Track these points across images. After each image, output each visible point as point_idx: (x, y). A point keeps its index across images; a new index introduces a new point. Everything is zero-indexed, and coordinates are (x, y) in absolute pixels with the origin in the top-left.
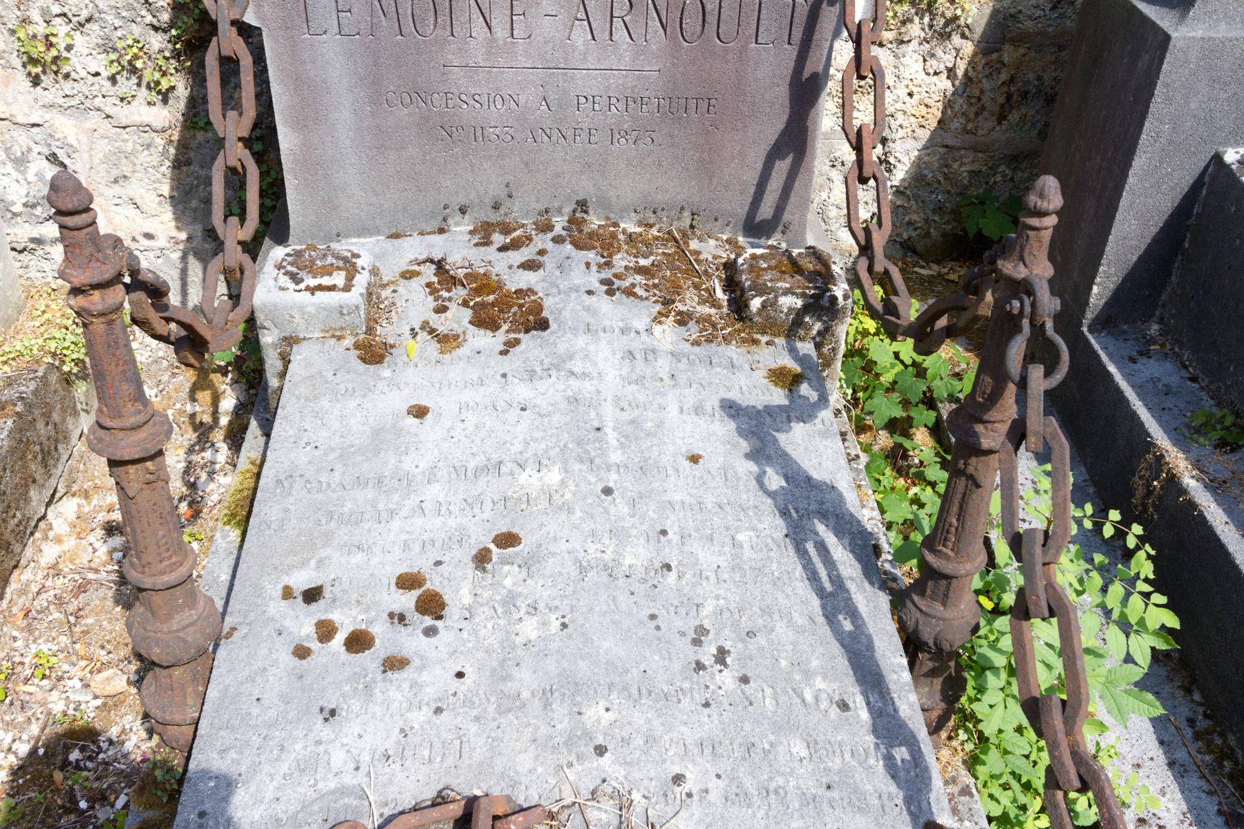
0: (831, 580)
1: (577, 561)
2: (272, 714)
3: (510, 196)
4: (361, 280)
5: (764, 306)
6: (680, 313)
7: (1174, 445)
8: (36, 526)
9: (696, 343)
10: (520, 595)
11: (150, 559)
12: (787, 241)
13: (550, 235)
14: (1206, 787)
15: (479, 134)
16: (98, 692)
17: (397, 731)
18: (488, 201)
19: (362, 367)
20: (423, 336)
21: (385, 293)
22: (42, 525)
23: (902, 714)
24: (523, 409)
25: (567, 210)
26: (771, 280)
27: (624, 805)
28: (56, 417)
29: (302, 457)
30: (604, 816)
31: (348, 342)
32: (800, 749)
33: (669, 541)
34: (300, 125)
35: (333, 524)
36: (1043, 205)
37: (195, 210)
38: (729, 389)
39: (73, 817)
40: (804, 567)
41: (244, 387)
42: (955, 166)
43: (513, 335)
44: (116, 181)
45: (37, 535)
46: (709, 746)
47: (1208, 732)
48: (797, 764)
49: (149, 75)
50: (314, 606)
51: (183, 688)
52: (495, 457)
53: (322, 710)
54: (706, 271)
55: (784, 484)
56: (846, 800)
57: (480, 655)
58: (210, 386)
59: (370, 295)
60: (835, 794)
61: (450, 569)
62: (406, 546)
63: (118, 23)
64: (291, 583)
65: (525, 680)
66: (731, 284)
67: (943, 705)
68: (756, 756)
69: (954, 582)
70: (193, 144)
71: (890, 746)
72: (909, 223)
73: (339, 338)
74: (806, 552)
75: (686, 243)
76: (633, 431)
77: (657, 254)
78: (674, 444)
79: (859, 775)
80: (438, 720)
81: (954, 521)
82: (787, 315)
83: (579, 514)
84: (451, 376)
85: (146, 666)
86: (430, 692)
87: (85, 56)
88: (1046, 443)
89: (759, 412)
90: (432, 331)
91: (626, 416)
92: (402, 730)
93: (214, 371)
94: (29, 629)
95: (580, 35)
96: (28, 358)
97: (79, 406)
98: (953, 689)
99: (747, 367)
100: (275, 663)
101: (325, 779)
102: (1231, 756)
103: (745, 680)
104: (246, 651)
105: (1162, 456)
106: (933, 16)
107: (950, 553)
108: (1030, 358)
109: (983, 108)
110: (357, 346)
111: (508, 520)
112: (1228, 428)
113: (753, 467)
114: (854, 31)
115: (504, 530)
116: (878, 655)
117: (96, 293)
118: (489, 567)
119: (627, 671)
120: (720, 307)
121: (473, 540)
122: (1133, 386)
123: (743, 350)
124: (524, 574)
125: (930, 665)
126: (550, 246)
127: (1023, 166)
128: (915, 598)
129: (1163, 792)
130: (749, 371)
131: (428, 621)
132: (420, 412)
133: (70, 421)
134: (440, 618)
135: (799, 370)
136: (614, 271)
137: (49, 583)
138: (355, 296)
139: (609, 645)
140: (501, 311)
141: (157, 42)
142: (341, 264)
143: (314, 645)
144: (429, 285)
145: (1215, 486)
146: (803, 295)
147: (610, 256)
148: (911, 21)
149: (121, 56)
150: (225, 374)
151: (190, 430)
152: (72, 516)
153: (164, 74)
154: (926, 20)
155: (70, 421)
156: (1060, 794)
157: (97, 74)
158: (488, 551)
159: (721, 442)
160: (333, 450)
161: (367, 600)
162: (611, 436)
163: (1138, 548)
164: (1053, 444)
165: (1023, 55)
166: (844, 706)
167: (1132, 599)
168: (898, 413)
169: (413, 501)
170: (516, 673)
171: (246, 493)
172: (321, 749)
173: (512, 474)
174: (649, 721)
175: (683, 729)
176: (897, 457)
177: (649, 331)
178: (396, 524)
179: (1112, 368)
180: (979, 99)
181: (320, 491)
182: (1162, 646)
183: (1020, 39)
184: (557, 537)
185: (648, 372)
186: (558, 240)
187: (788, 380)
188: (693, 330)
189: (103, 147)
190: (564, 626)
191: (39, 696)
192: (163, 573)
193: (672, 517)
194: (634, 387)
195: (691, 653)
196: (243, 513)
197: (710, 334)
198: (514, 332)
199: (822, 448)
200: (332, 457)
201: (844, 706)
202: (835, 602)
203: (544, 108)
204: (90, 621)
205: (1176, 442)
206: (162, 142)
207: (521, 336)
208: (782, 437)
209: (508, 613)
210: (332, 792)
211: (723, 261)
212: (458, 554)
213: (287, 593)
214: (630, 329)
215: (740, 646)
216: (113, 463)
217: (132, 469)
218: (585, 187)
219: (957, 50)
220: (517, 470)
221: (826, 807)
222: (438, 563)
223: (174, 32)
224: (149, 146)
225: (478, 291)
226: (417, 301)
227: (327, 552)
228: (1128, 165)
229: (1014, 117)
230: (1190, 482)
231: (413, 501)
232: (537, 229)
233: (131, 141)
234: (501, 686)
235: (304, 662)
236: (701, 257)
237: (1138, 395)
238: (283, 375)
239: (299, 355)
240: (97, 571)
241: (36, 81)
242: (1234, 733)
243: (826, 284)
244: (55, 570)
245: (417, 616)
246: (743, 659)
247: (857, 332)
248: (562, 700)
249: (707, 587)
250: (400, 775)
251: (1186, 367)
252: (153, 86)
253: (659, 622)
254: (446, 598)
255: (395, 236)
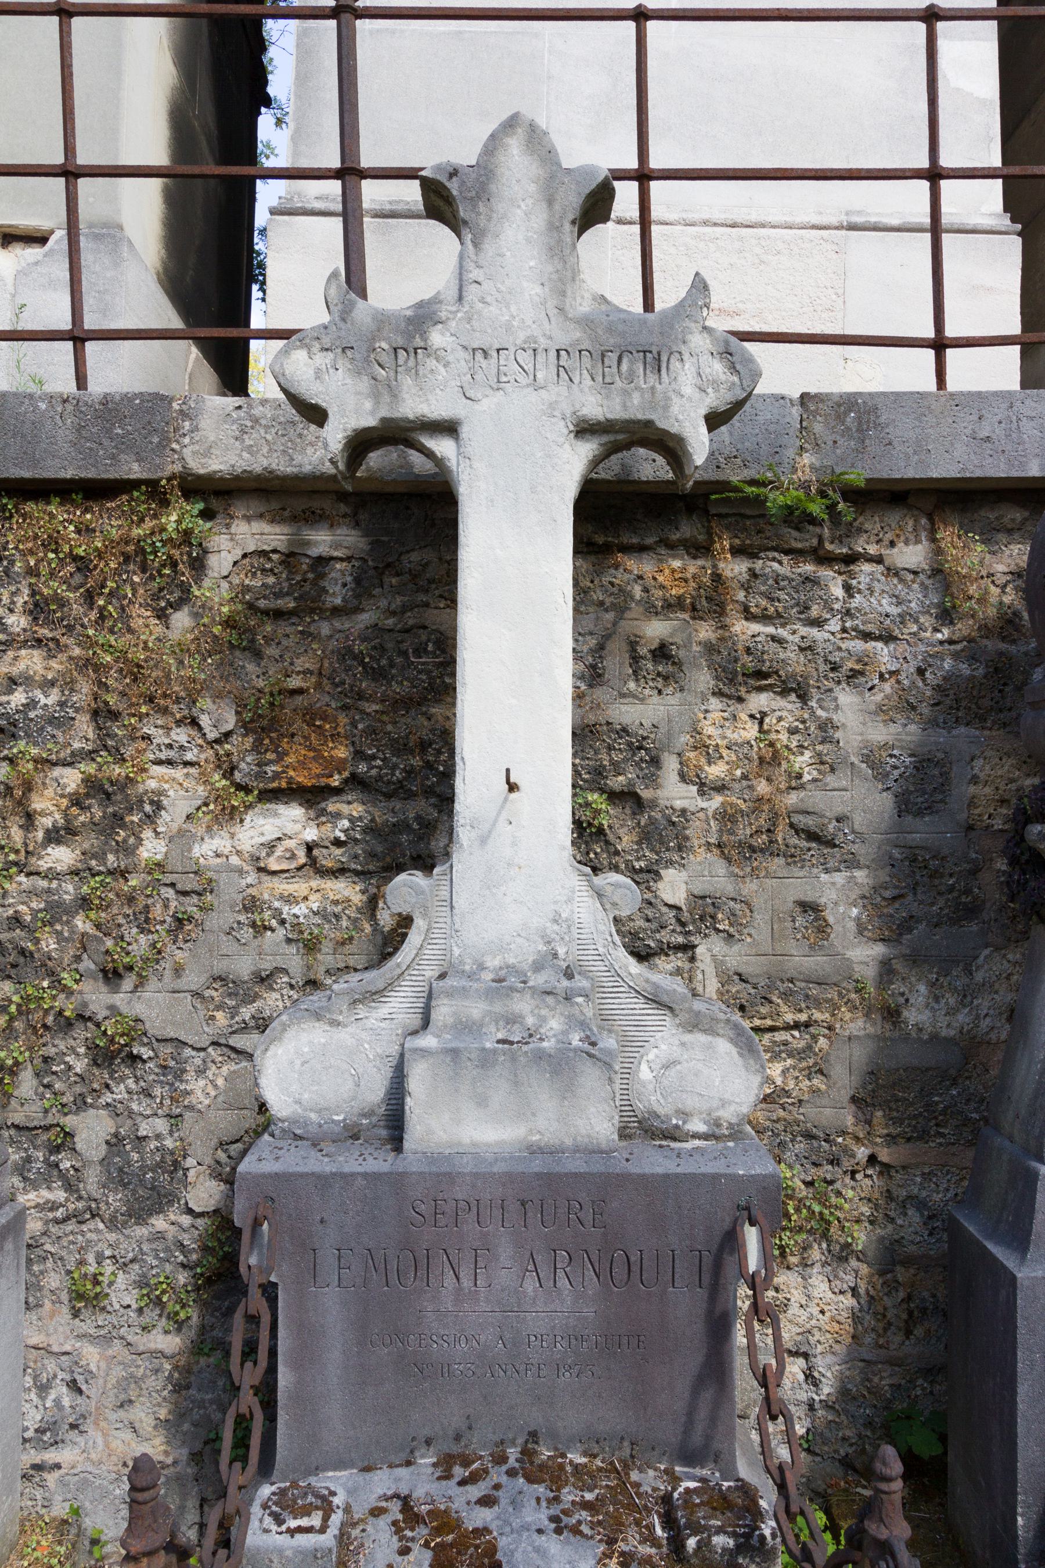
3: (470, 1428)
4: (336, 1519)
6: (623, 1554)
12: (720, 1471)
13: (504, 1468)
15: (445, 1370)
18: (451, 1433)
21: (355, 1532)
25: (520, 1441)
26: (704, 1518)
34: (298, 1365)
36: (887, 1472)
37: (185, 1434)
42: (876, 1379)
44: (122, 1406)
49: (172, 1307)
54: (646, 1506)
59: (343, 1538)
63: (155, 1263)
66: (669, 1521)
70: (195, 1369)
72: (844, 1439)
75: (627, 1474)
77: (601, 1487)
82: (722, 1555)
87: (122, 1292)
95: (530, 1285)
106: (829, 1242)
109: (890, 1324)
114: (750, 1281)
117: (145, 1560)
126: (504, 1479)
127: (940, 1378)
136: (561, 1506)
138: (327, 1539)
140: (459, 1553)
141: (182, 1278)
142: (319, 1503)
144: (395, 1523)
146: (734, 1535)
147: (559, 1490)
148: (810, 1247)
149: (152, 1291)
153: (183, 1307)
154: (824, 1245)
157: (129, 1306)
165: (915, 1275)
180: (884, 1316)
183: (907, 1262)
186: (511, 1473)
189: (118, 1372)
203: (501, 1346)
206: (169, 1367)
211: (662, 1493)
218: (535, 1418)
219: (856, 1272)
223: (199, 1270)
224: (157, 1371)
225: (438, 1531)
226: (383, 1541)
228: (1014, 1393)
229: (919, 1331)
232: (493, 1461)
233: (142, 1368)
236: (642, 1490)
241: (76, 1314)
243: (754, 1521)
252: (172, 1317)
255: (367, 1469)
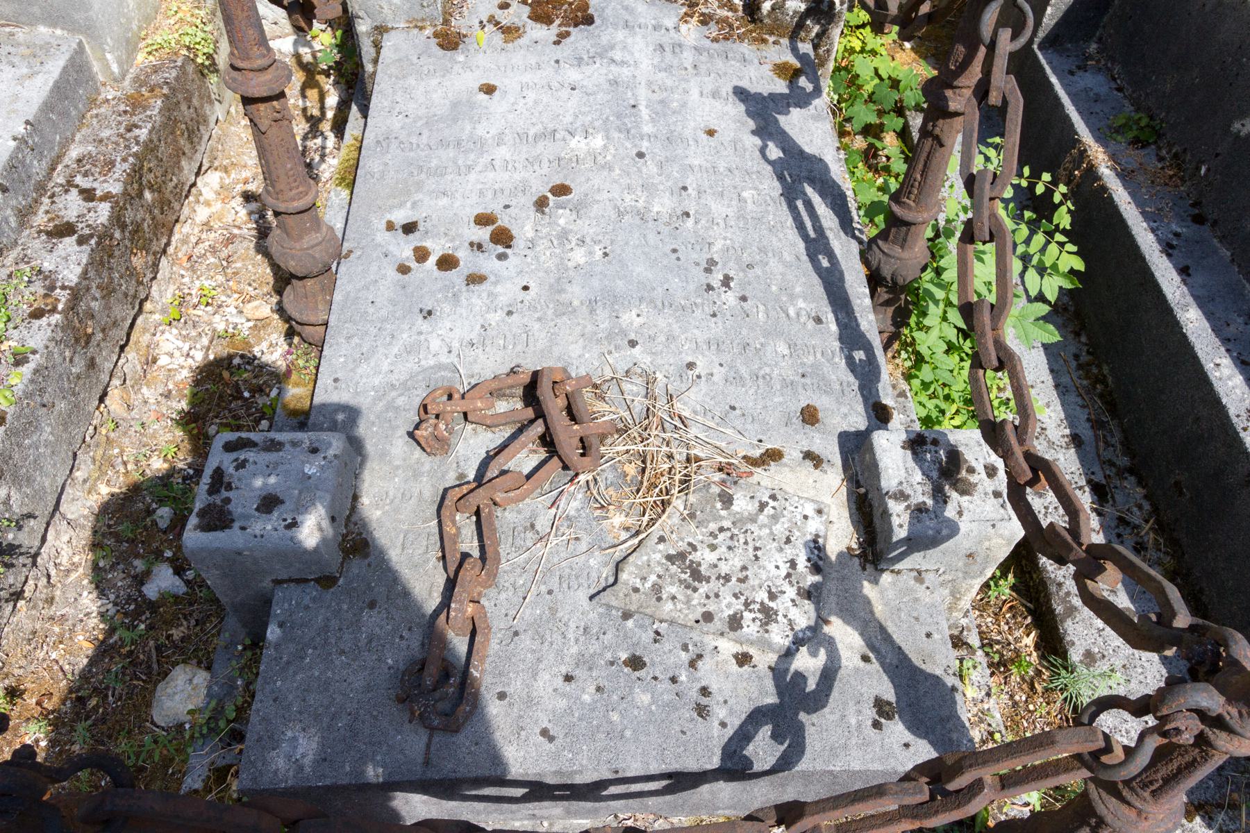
0: (815, 230)
1: (616, 207)
2: (384, 313)
5: (773, 8)
6: (703, 14)
7: (1097, 141)
8: (189, 191)
9: (715, 40)
10: (571, 231)
11: (282, 187)
14: (1080, 402)
16: (250, 316)
17: (479, 326)
19: (441, 52)
20: (490, 28)
22: (193, 190)
23: (862, 328)
24: (573, 89)
27: (650, 381)
28: (195, 102)
29: (396, 123)
30: (635, 388)
31: (429, 31)
32: (783, 349)
33: (689, 195)
35: (423, 176)
38: (740, 78)
39: (240, 403)
40: (794, 219)
41: (344, 87)
43: (564, 29)
45: (191, 198)
46: (716, 345)
47: (1088, 364)
48: (780, 359)
50: (411, 236)
51: (314, 296)
52: (551, 126)
53: (421, 311)
55: (782, 155)
56: (816, 386)
57: (541, 274)
58: (317, 85)
60: (808, 381)
61: (516, 211)
62: (481, 193)
64: (393, 219)
65: (576, 293)
67: (892, 329)
68: (750, 352)
69: (913, 228)
71: (851, 349)
73: (421, 28)
74: (796, 207)
76: (661, 109)
78: (695, 120)
79: (827, 369)
80: (510, 320)
81: (919, 177)
82: (792, 18)
83: (617, 172)
84: (514, 61)
85: (283, 280)
86: (503, 300)
88: (1004, 97)
89: (764, 98)
90: (497, 23)
91: (656, 97)
92: (483, 326)
93: (319, 73)
94: (193, 269)
96: (167, 50)
97: (213, 97)
98: (901, 319)
99: (756, 61)
100: (384, 277)
101: (426, 359)
102: (1103, 381)
103: (744, 299)
104: (361, 268)
105: (1085, 150)
107: (912, 203)
108: (1000, 24)
110: (436, 35)
111: (561, 175)
112: (1142, 128)
113: (758, 142)
115: (558, 182)
116: (847, 285)
118: (547, 210)
119: (654, 289)
120: (736, 11)
121: (534, 190)
122: (1069, 94)
123: (754, 47)
124: (574, 216)
125: (886, 296)
128: (880, 242)
129: (1048, 405)
130: (760, 67)
131: (500, 249)
132: (489, 90)
133: (207, 107)
134: (509, 247)
135: (799, 65)
137: (204, 236)
139: (640, 270)
140: (554, 8)
143: (413, 264)
145: (1125, 176)
150: (328, 76)
151: (304, 121)
152: (217, 187)
155: (207, 107)
156: (981, 372)
158: (547, 198)
159: (734, 121)
160: (420, 118)
161: (452, 233)
162: (644, 112)
163: (1061, 203)
164: (1010, 98)
166: (818, 320)
167: (1050, 247)
168: (873, 119)
169: (485, 159)
170: (568, 288)
171: (351, 162)
172: (422, 338)
173: (564, 140)
174: (670, 325)
175: (696, 331)
176: (870, 155)
177: (677, 28)
178: (473, 177)
179: (1054, 79)
181: (411, 150)
182: (1068, 285)
184: (602, 190)
185: (675, 62)
187: (792, 75)
188: (713, 30)
190: (606, 254)
191: (206, 318)
192: (293, 200)
193: (691, 177)
194: (663, 74)
195: (703, 278)
196: (349, 178)
197: (727, 33)
198: (565, 25)
199: (813, 128)
200: (419, 124)
201: (818, 320)
202: (817, 246)
204: (239, 265)
205: (1098, 139)
207: (571, 29)
208: (782, 119)
209: (562, 244)
210: (432, 368)
212: (523, 200)
213: (390, 226)
214: (661, 27)
215: (741, 274)
216: (247, 101)
217: (262, 107)
220: (568, 137)
221: (800, 390)
222: (507, 207)
227: (420, 196)
230: (1106, 172)
231: (485, 159)
234: (557, 297)
235: (406, 277)
237: (1072, 101)
238: (375, 61)
239: (388, 42)
240: (240, 228)
242: (1108, 364)
244: (207, 226)
245: (492, 245)
246: (742, 285)
247: (846, 50)
248: (604, 308)
249: (717, 231)
250: (482, 357)
251: (1114, 79)
253: (679, 254)
254: (513, 232)
